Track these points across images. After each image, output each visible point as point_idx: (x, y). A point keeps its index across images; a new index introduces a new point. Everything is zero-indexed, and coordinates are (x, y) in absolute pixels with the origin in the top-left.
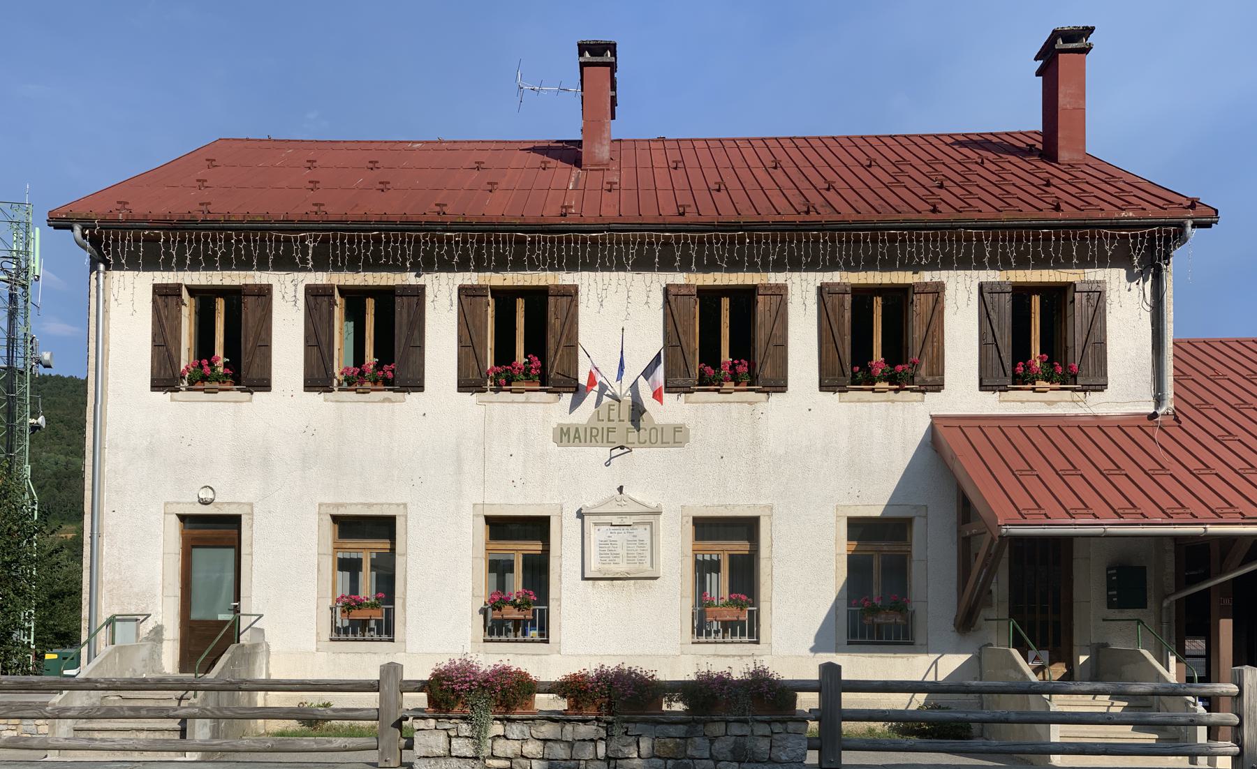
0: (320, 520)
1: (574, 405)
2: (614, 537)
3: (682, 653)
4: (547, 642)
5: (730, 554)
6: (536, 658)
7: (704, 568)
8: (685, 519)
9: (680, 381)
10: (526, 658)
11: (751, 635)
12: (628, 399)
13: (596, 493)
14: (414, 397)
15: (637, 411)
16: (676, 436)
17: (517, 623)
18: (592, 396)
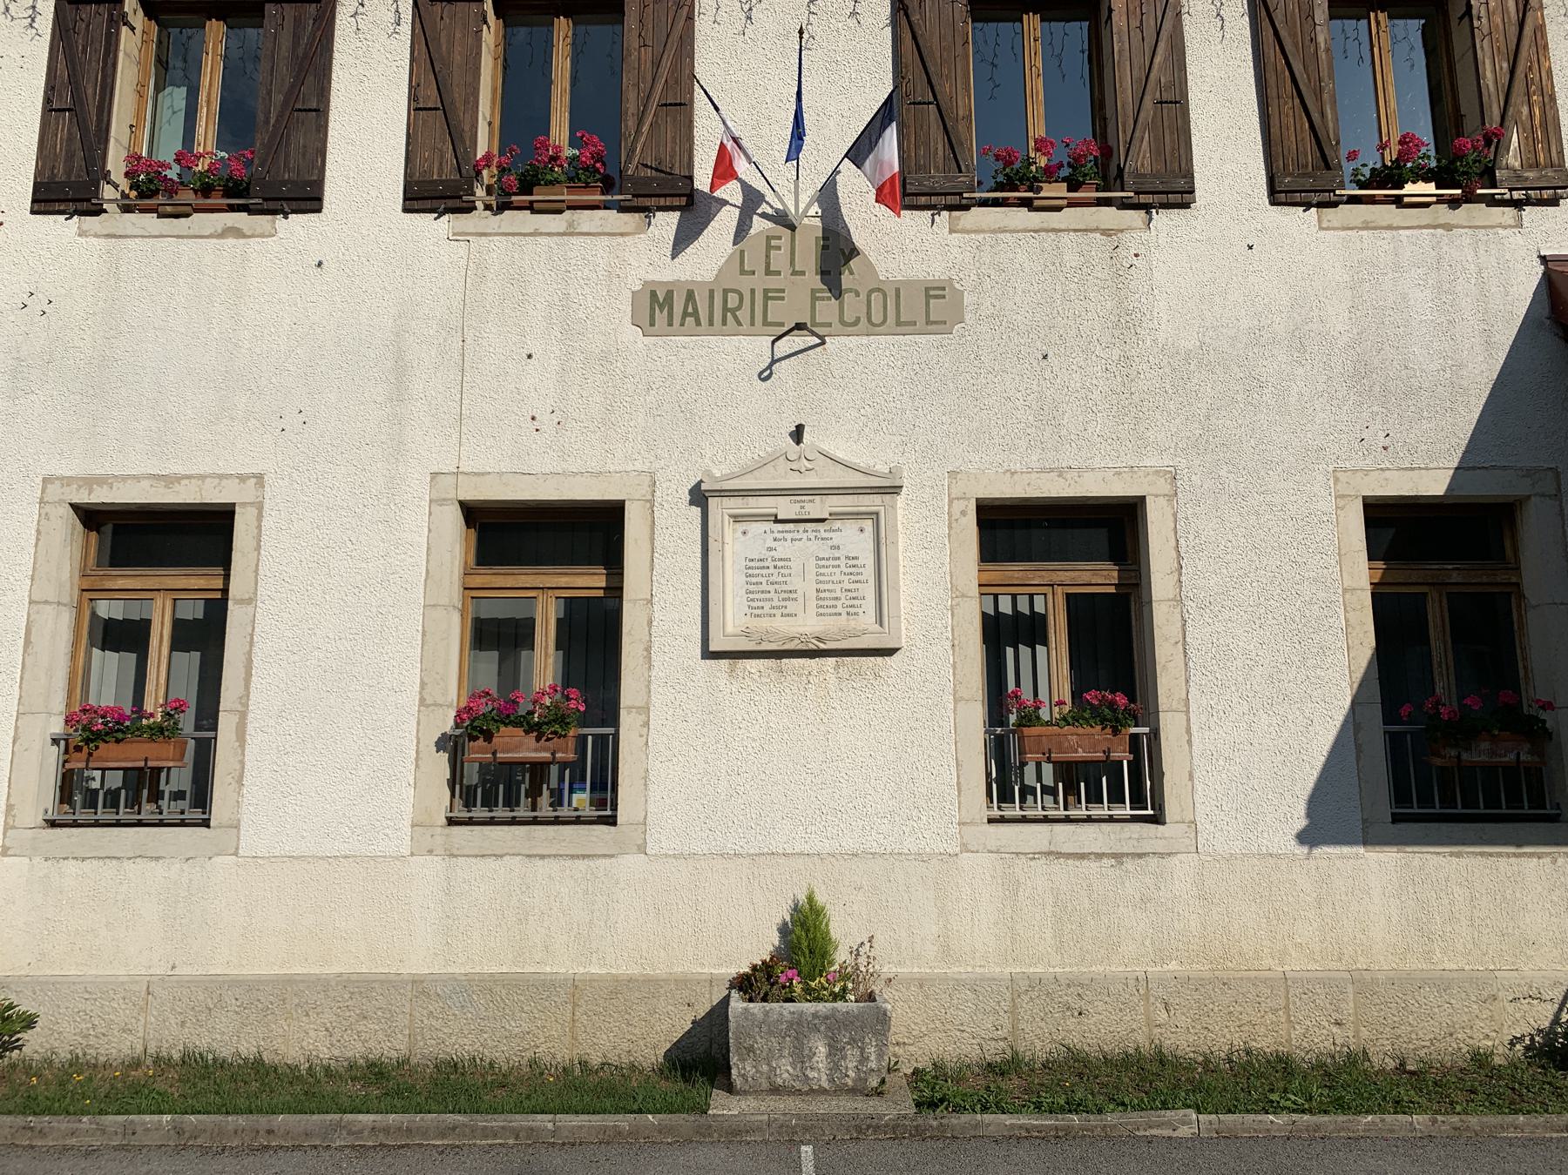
0: (44, 517)
1: (683, 239)
2: (783, 550)
3: (965, 848)
4: (611, 821)
5: (1073, 610)
6: (581, 864)
7: (1005, 633)
8: (958, 506)
9: (936, 178)
10: (553, 866)
11: (1138, 800)
12: (811, 220)
13: (738, 442)
14: (297, 224)
15: (836, 251)
16: (930, 307)
17: (538, 771)
18: (726, 220)
